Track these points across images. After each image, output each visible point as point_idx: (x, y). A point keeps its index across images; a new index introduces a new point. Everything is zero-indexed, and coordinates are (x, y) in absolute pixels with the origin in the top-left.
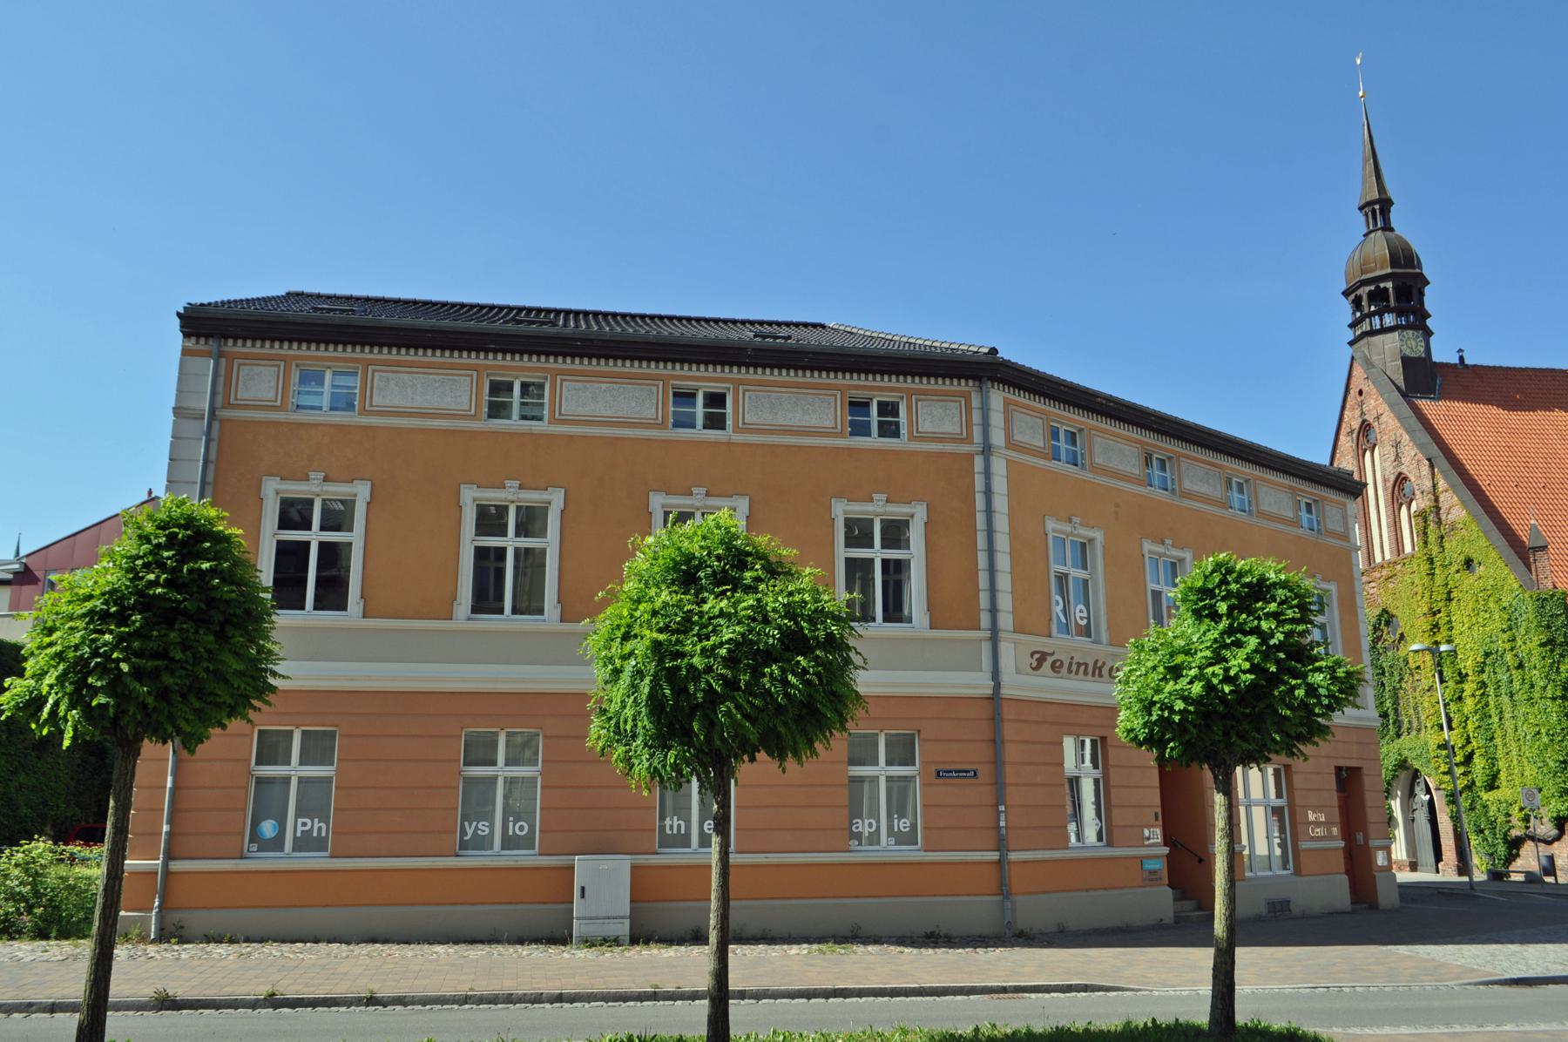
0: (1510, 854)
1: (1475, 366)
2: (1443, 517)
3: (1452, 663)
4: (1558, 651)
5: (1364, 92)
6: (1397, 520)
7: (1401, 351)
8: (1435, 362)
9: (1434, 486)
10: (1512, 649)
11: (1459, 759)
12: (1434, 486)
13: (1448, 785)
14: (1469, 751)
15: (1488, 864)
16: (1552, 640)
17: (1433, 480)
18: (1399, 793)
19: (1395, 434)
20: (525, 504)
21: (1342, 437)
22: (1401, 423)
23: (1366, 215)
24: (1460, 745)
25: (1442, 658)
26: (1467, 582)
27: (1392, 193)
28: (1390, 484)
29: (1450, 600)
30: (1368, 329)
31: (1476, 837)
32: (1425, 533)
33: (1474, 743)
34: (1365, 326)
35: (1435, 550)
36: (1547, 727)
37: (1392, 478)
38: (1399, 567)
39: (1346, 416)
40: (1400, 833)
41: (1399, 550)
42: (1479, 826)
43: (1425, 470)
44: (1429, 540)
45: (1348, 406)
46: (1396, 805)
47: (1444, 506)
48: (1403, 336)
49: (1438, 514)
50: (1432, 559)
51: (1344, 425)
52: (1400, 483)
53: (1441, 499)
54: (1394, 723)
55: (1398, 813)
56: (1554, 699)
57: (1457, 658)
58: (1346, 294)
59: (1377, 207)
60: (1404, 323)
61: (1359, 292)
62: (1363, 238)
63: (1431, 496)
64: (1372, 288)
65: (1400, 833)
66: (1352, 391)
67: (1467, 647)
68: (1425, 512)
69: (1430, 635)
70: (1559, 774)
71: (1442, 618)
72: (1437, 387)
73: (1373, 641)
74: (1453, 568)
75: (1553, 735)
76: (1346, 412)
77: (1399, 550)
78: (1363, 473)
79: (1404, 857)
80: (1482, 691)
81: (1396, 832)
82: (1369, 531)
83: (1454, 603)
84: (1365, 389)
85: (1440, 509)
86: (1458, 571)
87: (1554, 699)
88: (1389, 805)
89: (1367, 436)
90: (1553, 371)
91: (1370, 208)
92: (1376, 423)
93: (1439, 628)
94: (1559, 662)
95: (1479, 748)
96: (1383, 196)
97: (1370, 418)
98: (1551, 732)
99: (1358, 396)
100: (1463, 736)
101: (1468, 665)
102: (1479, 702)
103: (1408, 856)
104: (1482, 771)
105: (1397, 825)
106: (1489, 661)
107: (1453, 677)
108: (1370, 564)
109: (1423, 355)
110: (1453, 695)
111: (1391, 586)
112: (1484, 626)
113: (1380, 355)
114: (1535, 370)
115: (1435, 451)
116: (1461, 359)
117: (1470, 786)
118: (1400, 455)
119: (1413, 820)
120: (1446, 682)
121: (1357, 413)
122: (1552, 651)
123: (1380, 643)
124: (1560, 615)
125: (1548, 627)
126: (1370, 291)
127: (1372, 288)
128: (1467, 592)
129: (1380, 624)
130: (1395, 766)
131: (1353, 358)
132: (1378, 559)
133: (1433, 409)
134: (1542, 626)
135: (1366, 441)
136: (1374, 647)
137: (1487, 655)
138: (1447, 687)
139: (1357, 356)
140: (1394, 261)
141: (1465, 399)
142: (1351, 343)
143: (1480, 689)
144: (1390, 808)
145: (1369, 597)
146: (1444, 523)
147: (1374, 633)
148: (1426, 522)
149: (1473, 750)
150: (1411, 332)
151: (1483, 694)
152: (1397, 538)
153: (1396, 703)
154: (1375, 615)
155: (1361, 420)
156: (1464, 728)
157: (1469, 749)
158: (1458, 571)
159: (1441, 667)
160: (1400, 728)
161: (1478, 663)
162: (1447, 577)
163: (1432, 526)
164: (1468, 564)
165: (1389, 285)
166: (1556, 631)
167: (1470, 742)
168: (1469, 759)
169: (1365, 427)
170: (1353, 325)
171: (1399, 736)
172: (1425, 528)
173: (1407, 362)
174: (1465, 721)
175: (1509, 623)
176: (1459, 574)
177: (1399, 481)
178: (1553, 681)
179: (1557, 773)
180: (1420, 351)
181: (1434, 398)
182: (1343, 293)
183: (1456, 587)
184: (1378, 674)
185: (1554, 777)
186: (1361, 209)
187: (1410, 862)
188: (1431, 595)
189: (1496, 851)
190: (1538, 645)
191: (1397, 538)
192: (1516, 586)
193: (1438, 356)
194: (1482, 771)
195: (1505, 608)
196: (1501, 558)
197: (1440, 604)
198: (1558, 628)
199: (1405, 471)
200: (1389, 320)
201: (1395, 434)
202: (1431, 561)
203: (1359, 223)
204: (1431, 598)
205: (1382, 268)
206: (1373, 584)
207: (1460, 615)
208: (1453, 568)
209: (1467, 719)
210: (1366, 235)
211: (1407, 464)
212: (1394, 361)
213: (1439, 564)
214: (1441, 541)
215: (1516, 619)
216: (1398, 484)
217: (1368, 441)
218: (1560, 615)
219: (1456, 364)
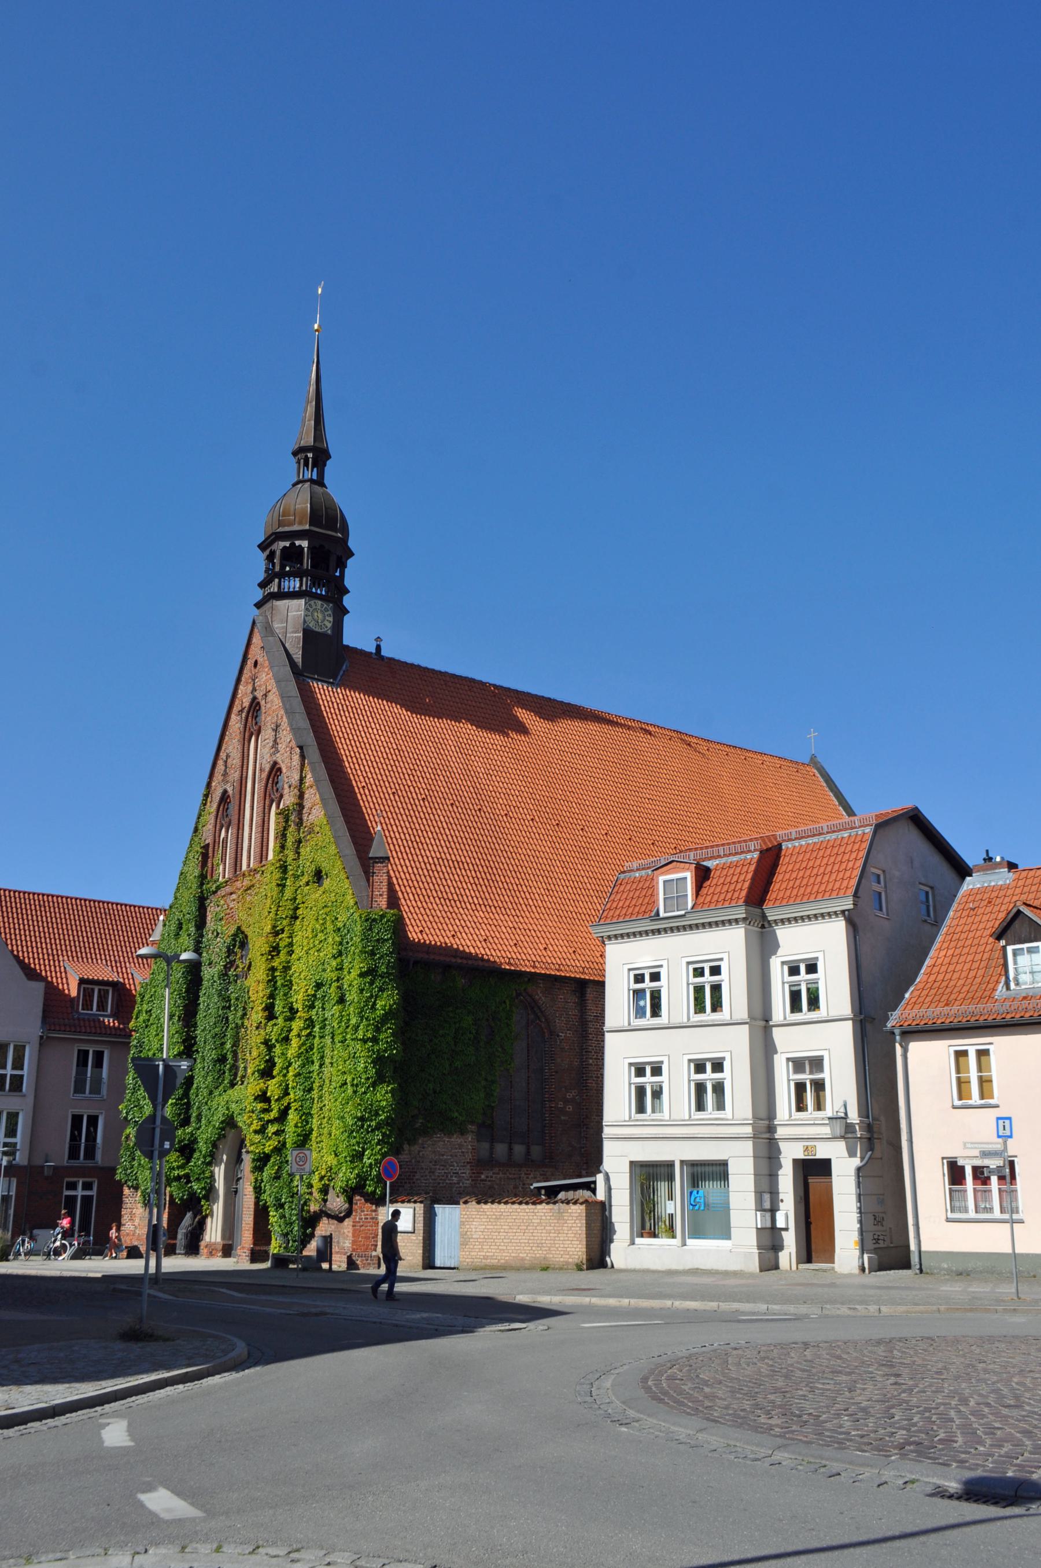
0: (304, 1234)
1: (391, 660)
2: (305, 818)
3: (285, 995)
4: (377, 983)
5: (319, 326)
6: (266, 819)
7: (305, 621)
8: (347, 647)
9: (302, 779)
10: (338, 980)
11: (274, 1114)
12: (302, 779)
13: (257, 1148)
14: (286, 1104)
15: (280, 1247)
16: (373, 970)
17: (301, 772)
18: (225, 1157)
19: (277, 716)
20: (947, 1187)
21: (233, 716)
22: (283, 702)
23: (299, 462)
24: (276, 1097)
25: (276, 989)
26: (313, 896)
27: (333, 442)
28: (265, 775)
29: (295, 917)
30: (276, 590)
31: (275, 1213)
32: (284, 836)
33: (292, 1096)
34: (274, 588)
35: (291, 855)
36: (353, 1076)
37: (267, 768)
38: (258, 876)
39: (240, 691)
40: (218, 1208)
41: (262, 856)
42: (280, 1199)
43: (296, 758)
44: (287, 844)
45: (243, 679)
46: (219, 1172)
47: (307, 804)
48: (310, 605)
49: (300, 813)
50: (286, 866)
51: (237, 702)
52: (275, 775)
53: (306, 796)
54: (230, 1070)
55: (220, 1184)
56: (364, 1041)
57: (291, 989)
58: (262, 547)
59: (310, 455)
60: (324, 593)
61: (274, 547)
62: (807, 761)
63: (296, 791)
64: (287, 544)
65: (218, 1208)
66: (249, 662)
67: (302, 976)
68: (288, 810)
69: (267, 959)
70: (354, 1134)
71: (284, 940)
72: (341, 673)
73: (225, 966)
74: (305, 879)
75: (357, 1086)
76: (241, 687)
77: (262, 856)
78: (245, 761)
79: (219, 1239)
80: (308, 1031)
81: (215, 1207)
82: (240, 831)
83: (298, 922)
84: (260, 660)
85: (303, 808)
86: (307, 884)
87: (364, 1041)
88: (212, 1172)
89: (256, 717)
90: (472, 681)
91: (303, 455)
92: (264, 701)
93: (279, 952)
94: (377, 996)
95: (295, 1101)
96: (318, 445)
97: (259, 694)
98: (355, 1082)
99: (253, 668)
100: (281, 1085)
101: (298, 999)
102: (303, 1044)
103: (223, 1237)
104: (294, 1129)
105: (216, 1200)
106: (319, 994)
107: (283, 1012)
108: (236, 871)
109: (329, 632)
110: (280, 1035)
111: (248, 898)
112: (319, 951)
113: (282, 623)
114: (453, 676)
115: (310, 739)
116: (378, 648)
117: (279, 1150)
118: (278, 740)
119: (236, 1192)
120: (277, 1018)
121: (250, 687)
122: (372, 983)
123: (232, 970)
124: (387, 940)
125: (372, 953)
126: (285, 547)
127: (287, 544)
128: (311, 908)
129: (234, 946)
130: (222, 1122)
131: (254, 623)
132: (244, 867)
133: (323, 692)
134: (365, 952)
135: (254, 722)
136: (226, 974)
137: (319, 986)
138: (275, 1025)
139: (260, 620)
140: (315, 517)
141: (367, 692)
142: (259, 605)
143: (306, 1028)
144: (212, 1176)
145: (228, 911)
146: (304, 825)
147: (228, 957)
148: (287, 821)
149: (289, 1104)
150: (319, 602)
151: (309, 1034)
152: (262, 841)
153: (236, 1044)
154: (230, 933)
155: (251, 696)
156: (285, 1076)
157: (285, 1102)
158: (307, 884)
159: (274, 999)
160: (236, 1075)
161: (308, 996)
162: (296, 890)
163: (292, 828)
164: (319, 876)
165: (305, 544)
166: (379, 959)
167: (289, 1094)
168: (284, 1114)
169: (255, 707)
170: (263, 585)
171: (232, 1085)
172: (285, 829)
173: (309, 635)
174: (287, 1068)
175: (340, 947)
176: (308, 888)
177: (274, 773)
178: (366, 1019)
179: (352, 1132)
180: (324, 622)
181: (332, 684)
182: (259, 546)
183: (303, 903)
184: (224, 1008)
185: (348, 1137)
186: (295, 454)
187: (224, 1246)
188: (277, 910)
189: (291, 1231)
190: (358, 975)
191: (262, 841)
192: (352, 902)
193: (350, 638)
194: (294, 1129)
195: (339, 929)
196: (344, 868)
197: (285, 922)
198: (382, 956)
199: (279, 761)
200: (294, 584)
201: (277, 716)
202: (284, 869)
203: (290, 471)
204: (276, 914)
205: (300, 523)
206: (234, 896)
207: (302, 936)
208: (305, 879)
209: (290, 1064)
210: (294, 485)
211: (282, 751)
212: (295, 633)
213: (291, 873)
214: (298, 847)
215: (348, 943)
216: (272, 776)
217: (256, 723)
218: (387, 940)
219: (371, 653)
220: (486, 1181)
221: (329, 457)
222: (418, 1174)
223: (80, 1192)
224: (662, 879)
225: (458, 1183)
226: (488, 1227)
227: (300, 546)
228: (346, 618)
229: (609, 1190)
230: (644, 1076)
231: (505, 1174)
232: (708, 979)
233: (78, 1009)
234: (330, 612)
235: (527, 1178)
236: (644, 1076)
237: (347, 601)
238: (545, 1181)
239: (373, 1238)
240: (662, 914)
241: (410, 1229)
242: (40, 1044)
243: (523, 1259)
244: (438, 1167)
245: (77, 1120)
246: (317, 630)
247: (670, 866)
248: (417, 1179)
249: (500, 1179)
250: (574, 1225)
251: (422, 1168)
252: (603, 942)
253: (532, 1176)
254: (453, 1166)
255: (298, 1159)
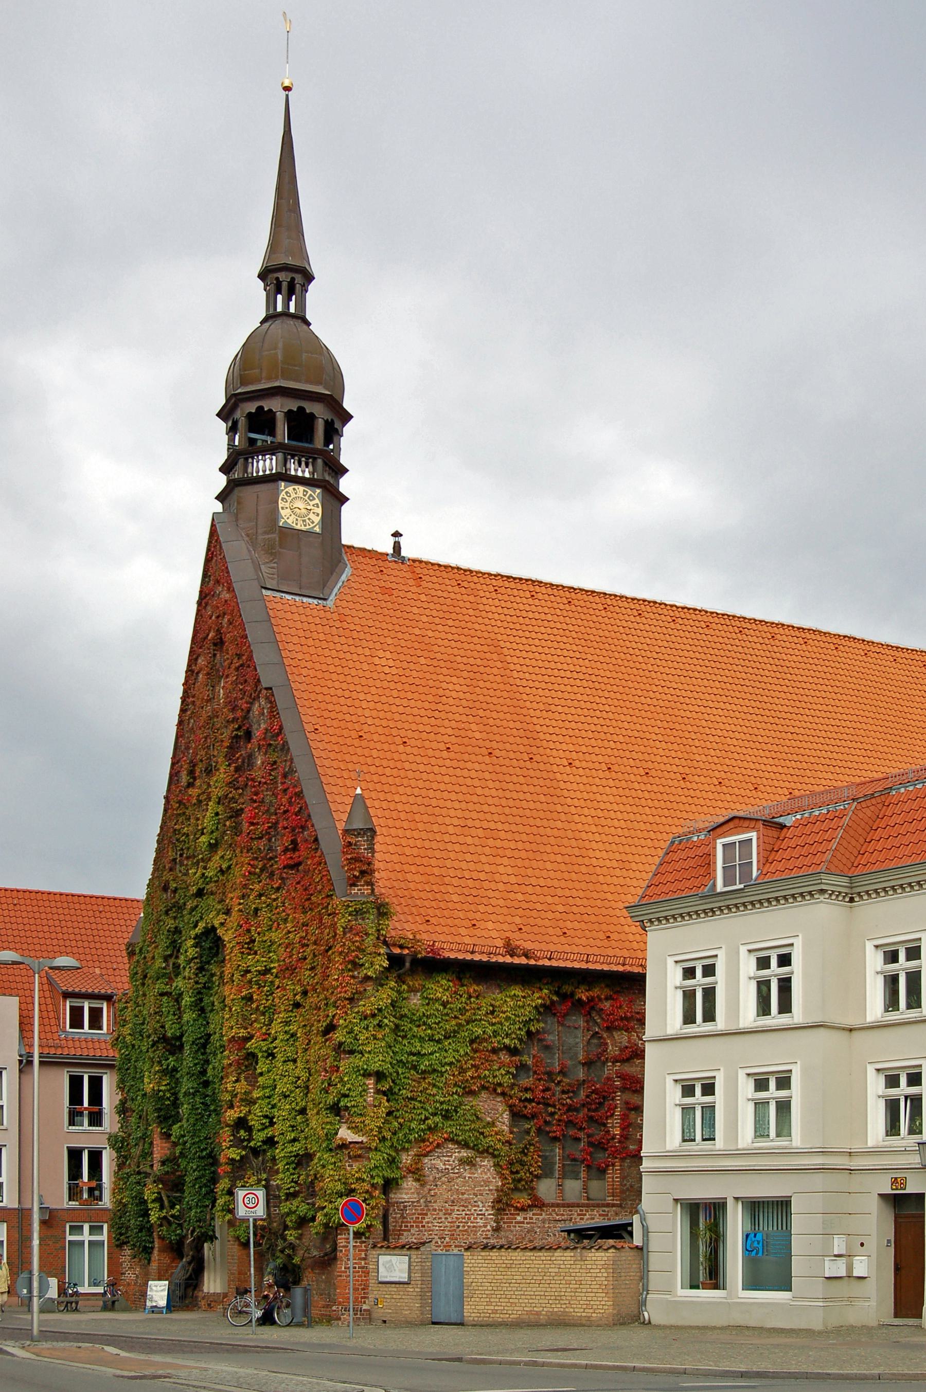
58: (223, 414)
109: (317, 529)
116: (397, 547)
170: (224, 469)
220: (523, 1223)
221: (309, 278)
222: (429, 1216)
223: (86, 1236)
224: (720, 843)
225: (485, 1226)
226: (497, 1277)
227: (270, 410)
228: (345, 509)
229: (646, 1232)
230: (767, 1089)
231: (551, 1214)
232: (903, 964)
233: (65, 1027)
234: (317, 501)
235: (581, 1219)
236: (767, 1089)
237: (345, 485)
238: (254, 1242)
239: (363, 1289)
240: (720, 887)
241: (404, 1277)
242: (20, 1071)
243: (538, 1313)
244: (456, 1208)
245: (75, 1155)
246: (298, 527)
247: (731, 825)
248: (428, 1223)
249: (544, 1221)
250: (600, 1275)
251: (435, 1210)
252: (644, 928)
253: (588, 1216)
254: (478, 1206)
255: (246, 1201)
